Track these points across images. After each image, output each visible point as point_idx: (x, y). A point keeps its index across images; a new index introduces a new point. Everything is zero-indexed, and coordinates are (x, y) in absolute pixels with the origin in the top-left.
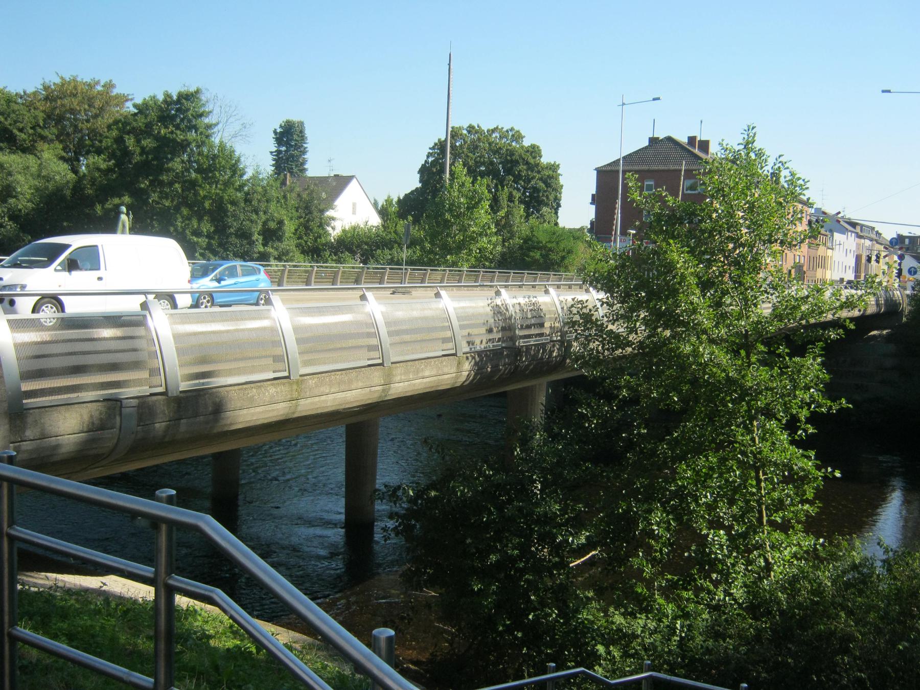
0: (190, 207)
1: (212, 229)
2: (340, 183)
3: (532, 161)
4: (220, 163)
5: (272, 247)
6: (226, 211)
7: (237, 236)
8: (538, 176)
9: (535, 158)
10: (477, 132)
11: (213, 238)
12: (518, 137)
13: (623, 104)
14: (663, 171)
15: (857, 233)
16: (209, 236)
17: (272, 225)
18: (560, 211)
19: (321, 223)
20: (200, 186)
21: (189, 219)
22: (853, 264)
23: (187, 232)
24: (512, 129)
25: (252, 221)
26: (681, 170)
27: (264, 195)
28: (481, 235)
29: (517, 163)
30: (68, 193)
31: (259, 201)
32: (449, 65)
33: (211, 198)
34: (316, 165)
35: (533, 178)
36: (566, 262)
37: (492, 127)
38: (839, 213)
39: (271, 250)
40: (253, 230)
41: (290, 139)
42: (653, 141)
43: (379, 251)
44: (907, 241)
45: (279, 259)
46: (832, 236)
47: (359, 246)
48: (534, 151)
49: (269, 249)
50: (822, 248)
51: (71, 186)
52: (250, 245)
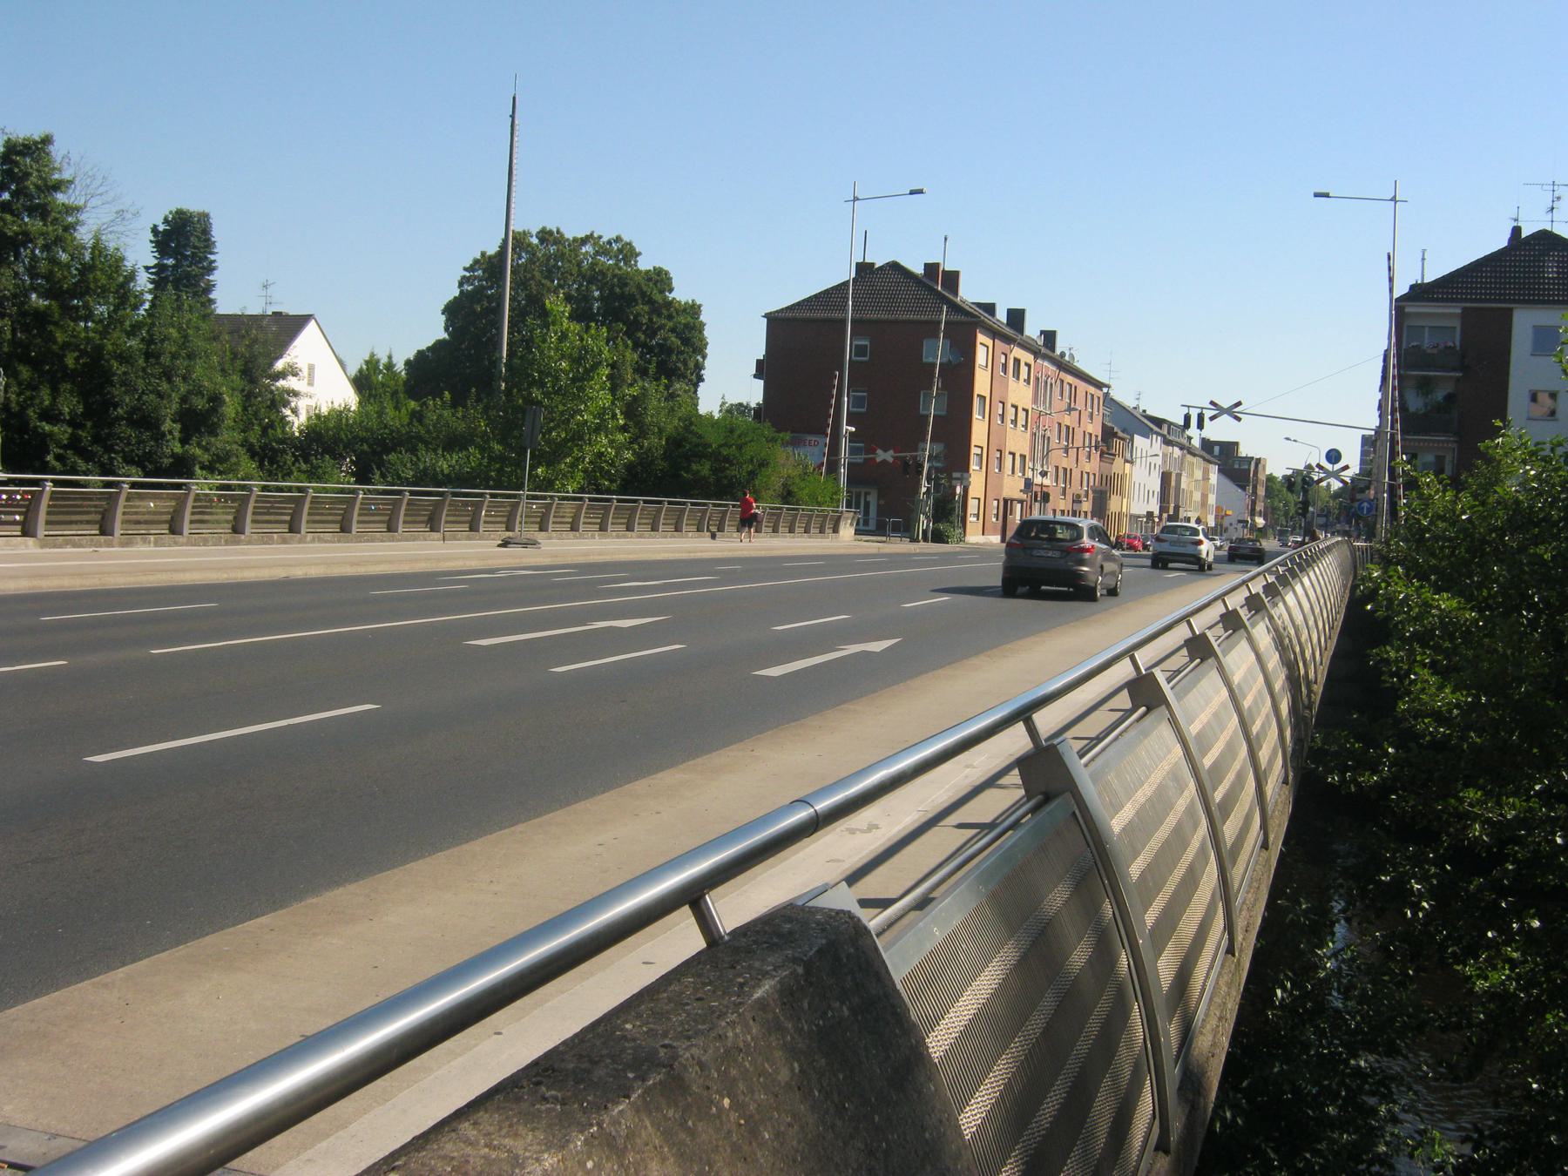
0: (35, 364)
1: (80, 410)
2: (289, 326)
3: (658, 297)
4: (96, 280)
5: (199, 445)
7: (132, 423)
8: (670, 324)
9: (662, 292)
10: (556, 242)
11: (82, 426)
12: (628, 253)
13: (856, 199)
14: (926, 322)
15: (1163, 436)
16: (73, 423)
17: (200, 404)
18: (702, 388)
19: (273, 401)
20: (56, 324)
21: (34, 388)
22: (1158, 489)
23: (30, 412)
24: (618, 239)
25: (160, 395)
26: (939, 323)
27: (183, 346)
29: (630, 300)
31: (174, 356)
32: (513, 117)
33: (77, 348)
34: (235, 291)
35: (662, 327)
37: (581, 235)
38: (1239, 404)
39: (198, 452)
41: (184, 241)
42: (864, 269)
43: (392, 457)
44: (1217, 449)
45: (210, 469)
46: (1132, 440)
47: (349, 446)
48: (661, 279)
50: (1119, 461)
52: (156, 440)
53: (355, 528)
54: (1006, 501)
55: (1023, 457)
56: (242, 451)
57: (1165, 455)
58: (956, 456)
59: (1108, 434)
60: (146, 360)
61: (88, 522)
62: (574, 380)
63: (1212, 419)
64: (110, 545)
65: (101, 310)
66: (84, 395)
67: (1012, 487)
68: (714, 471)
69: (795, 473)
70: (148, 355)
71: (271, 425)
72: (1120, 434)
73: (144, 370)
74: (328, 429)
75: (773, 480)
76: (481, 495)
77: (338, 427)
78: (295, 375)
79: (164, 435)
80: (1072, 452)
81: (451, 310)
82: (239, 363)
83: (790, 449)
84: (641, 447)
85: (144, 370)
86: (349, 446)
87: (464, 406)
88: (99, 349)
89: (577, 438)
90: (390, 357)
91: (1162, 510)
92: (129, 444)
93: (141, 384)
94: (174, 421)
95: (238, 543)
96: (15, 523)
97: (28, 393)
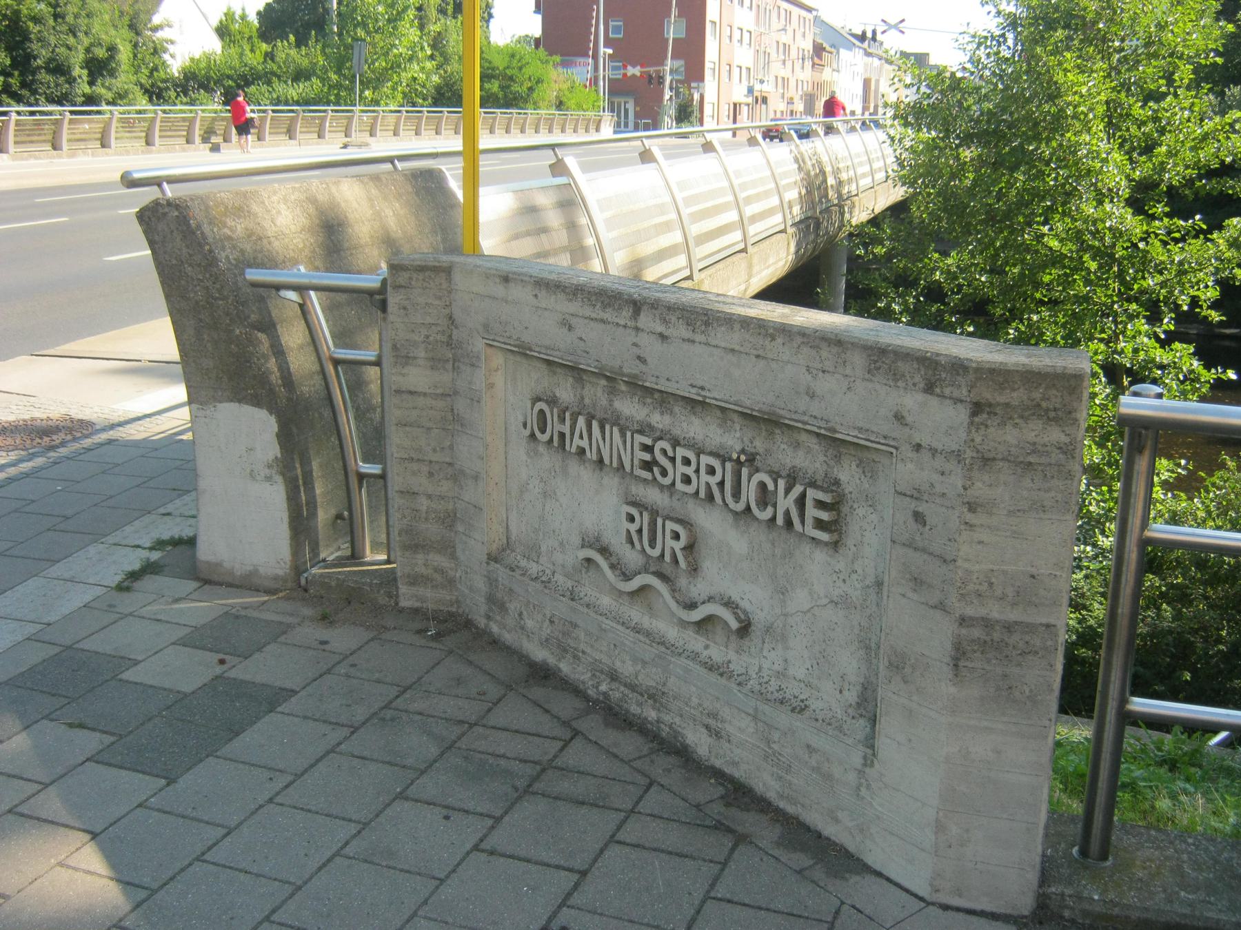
5: (103, 85)
7: (49, 71)
11: (11, 75)
17: (101, 53)
22: (860, 92)
25: (69, 48)
28: (411, 59)
31: (76, 16)
36: (535, 95)
38: (903, 21)
39: (103, 91)
40: (72, 61)
46: (838, 52)
47: (218, 82)
49: (99, 90)
50: (827, 70)
52: (70, 83)
53: (327, 135)
54: (735, 105)
55: (749, 69)
56: (137, 89)
57: (866, 65)
58: (695, 71)
59: (818, 50)
60: (55, 20)
61: (44, 141)
62: (389, 21)
63: (884, 32)
64: (60, 157)
67: (739, 93)
68: (502, 88)
69: (565, 87)
70: (56, 16)
71: (155, 69)
72: (828, 48)
73: (54, 28)
74: (200, 70)
75: (549, 92)
76: (325, 111)
77: (209, 68)
78: (170, 26)
79: (75, 79)
80: (789, 64)
82: (126, 20)
83: (560, 69)
84: (446, 72)
85: (54, 28)
86: (218, 82)
87: (307, 46)
88: (17, 13)
89: (395, 66)
91: (865, 109)
93: (53, 40)
94: (82, 68)
95: (150, 152)
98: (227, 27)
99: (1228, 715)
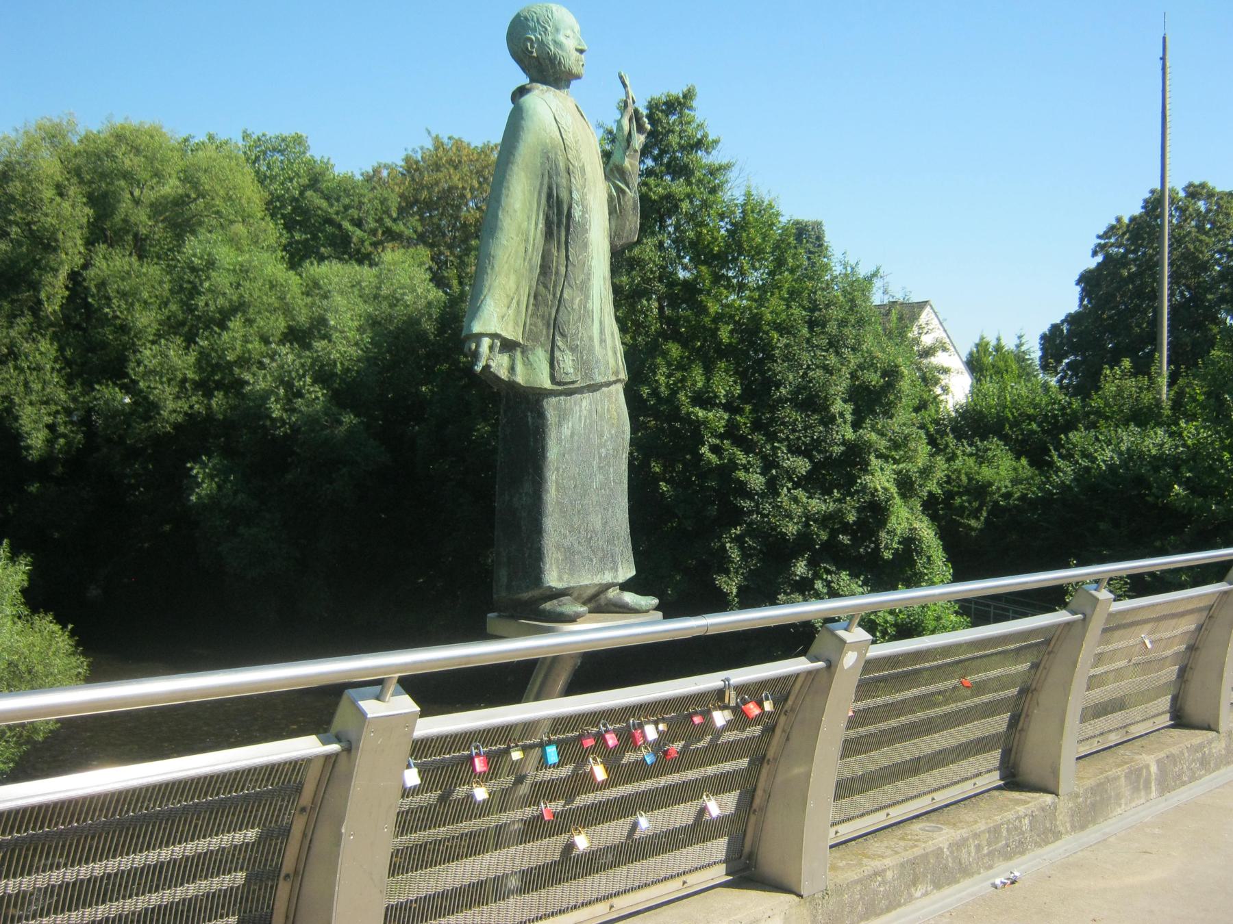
0: (684, 342)
5: (873, 429)
6: (768, 348)
11: (739, 411)
17: (874, 379)
23: (682, 396)
25: (828, 370)
30: (428, 326)
31: (843, 323)
32: (1163, 59)
39: (874, 436)
43: (1075, 436)
51: (435, 313)
52: (826, 425)
60: (811, 329)
65: (755, 277)
66: (742, 375)
70: (812, 324)
73: (808, 341)
78: (945, 349)
81: (1088, 281)
85: (808, 341)
88: (756, 319)
90: (998, 339)
92: (794, 431)
93: (806, 358)
94: (845, 401)
96: (700, 830)
97: (679, 375)
98: (978, 360)
99: (983, 589)
